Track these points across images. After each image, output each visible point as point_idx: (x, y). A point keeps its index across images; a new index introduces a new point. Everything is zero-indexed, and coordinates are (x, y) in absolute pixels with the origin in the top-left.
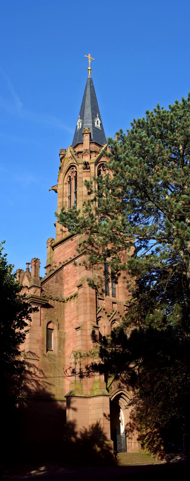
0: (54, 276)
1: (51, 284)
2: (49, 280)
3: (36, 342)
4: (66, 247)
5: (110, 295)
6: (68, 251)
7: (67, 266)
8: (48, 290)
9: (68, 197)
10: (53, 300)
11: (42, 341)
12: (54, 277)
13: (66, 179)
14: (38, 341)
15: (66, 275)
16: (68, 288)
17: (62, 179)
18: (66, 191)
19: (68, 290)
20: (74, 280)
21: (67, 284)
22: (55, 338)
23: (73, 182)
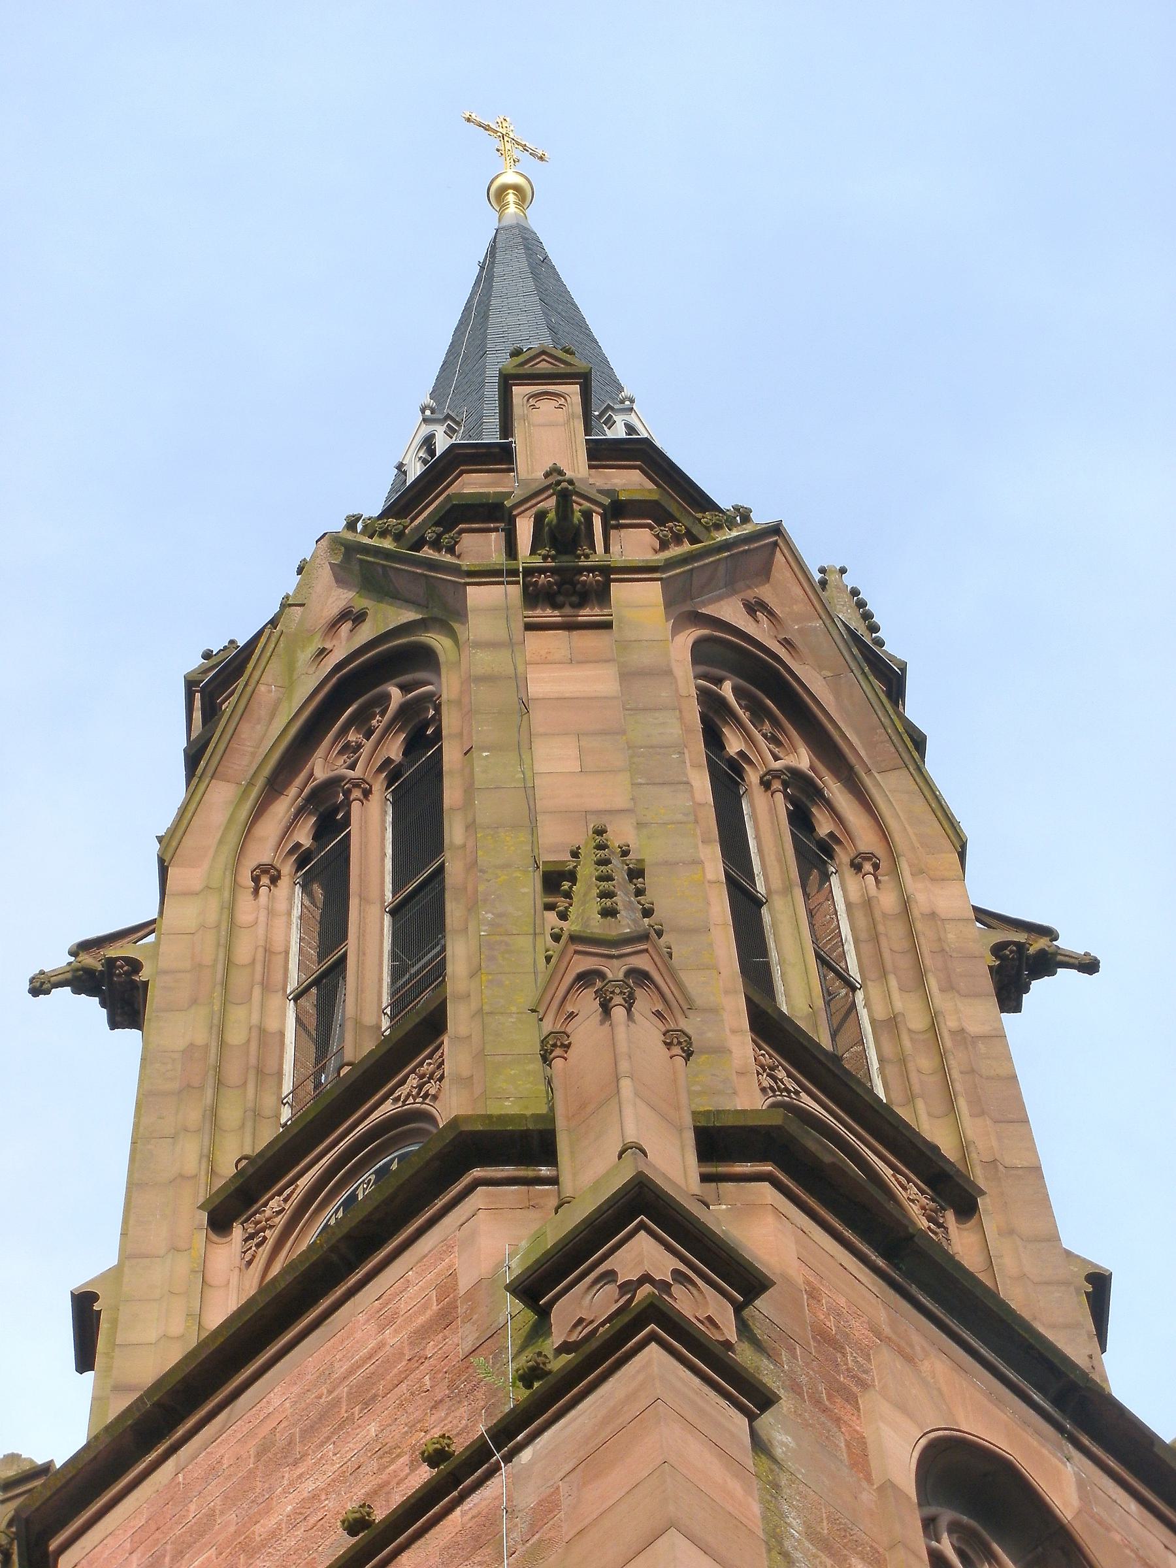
6: (309, 1486)
17: (221, 842)
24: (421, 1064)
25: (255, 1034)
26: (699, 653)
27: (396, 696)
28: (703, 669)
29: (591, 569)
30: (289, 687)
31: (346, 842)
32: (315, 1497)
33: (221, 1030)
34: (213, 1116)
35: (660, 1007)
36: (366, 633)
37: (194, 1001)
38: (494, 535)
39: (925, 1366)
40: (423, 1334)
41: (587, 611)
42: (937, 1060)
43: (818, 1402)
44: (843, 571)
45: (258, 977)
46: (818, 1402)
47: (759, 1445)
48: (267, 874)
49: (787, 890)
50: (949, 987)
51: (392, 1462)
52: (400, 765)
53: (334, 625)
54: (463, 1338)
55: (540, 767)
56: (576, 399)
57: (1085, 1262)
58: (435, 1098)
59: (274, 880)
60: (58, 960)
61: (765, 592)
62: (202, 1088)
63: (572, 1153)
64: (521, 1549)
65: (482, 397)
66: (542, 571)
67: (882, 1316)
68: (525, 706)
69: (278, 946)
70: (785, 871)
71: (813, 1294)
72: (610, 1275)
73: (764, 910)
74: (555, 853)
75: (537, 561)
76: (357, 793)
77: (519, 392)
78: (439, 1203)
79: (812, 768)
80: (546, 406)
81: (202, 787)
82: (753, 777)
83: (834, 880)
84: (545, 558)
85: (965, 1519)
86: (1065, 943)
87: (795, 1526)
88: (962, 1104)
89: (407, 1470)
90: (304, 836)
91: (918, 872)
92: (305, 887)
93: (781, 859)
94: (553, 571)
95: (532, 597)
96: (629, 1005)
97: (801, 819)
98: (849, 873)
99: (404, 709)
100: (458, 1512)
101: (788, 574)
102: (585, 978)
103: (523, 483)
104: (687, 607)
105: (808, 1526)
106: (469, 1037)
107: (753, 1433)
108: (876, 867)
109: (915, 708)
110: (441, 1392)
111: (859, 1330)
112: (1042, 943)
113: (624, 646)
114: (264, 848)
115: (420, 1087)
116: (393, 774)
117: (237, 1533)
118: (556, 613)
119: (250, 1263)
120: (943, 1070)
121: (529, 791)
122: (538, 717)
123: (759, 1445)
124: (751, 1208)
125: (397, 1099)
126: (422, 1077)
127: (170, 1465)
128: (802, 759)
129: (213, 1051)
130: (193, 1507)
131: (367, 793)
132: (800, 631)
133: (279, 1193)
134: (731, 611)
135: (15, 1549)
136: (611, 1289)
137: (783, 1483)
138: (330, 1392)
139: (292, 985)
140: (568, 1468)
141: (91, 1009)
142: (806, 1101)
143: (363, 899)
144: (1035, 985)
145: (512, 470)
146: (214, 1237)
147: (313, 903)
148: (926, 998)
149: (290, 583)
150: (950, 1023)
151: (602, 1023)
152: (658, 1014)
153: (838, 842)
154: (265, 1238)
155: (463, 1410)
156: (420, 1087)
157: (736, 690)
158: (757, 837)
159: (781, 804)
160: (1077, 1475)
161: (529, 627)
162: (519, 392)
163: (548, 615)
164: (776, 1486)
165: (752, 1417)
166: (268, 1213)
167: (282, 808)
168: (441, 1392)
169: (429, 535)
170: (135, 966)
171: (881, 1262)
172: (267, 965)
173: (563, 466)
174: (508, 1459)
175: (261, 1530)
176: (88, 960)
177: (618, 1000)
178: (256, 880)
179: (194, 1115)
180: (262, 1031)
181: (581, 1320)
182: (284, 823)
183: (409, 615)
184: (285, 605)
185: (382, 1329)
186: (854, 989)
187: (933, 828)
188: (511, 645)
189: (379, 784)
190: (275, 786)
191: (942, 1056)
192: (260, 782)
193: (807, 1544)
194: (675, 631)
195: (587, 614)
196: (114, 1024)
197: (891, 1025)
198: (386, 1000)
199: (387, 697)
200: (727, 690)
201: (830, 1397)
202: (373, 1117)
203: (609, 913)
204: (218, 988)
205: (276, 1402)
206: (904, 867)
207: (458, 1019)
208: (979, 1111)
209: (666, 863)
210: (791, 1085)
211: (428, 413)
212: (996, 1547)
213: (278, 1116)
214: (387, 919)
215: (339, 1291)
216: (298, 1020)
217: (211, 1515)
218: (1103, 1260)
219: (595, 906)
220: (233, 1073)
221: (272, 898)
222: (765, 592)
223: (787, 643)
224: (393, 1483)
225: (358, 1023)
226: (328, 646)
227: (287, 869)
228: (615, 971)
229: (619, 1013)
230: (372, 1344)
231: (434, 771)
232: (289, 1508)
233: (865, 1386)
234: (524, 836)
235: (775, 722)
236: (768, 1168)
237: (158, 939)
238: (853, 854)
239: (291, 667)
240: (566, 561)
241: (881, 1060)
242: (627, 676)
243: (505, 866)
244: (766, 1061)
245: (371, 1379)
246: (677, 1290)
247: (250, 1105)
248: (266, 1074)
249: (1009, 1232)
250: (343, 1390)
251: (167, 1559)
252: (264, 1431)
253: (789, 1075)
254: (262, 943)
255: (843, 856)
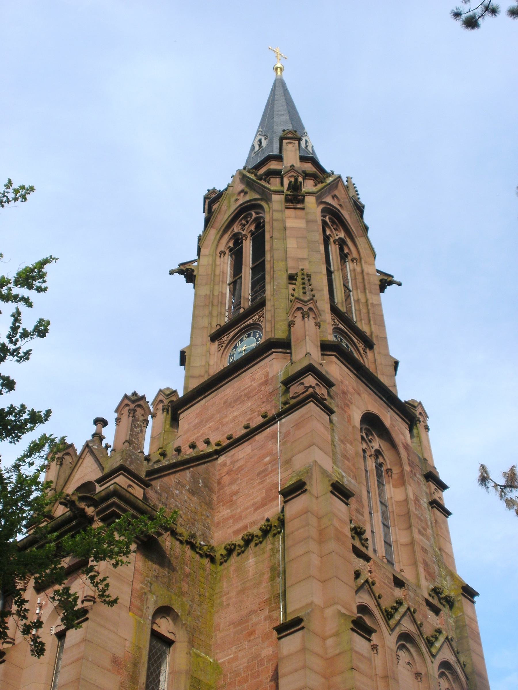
0: (187, 472)
1: (177, 492)
2: (172, 477)
3: (107, 663)
4: (228, 404)
5: (421, 560)
6: (236, 414)
7: (232, 452)
8: (166, 505)
9: (229, 285)
10: (181, 542)
11: (130, 666)
12: (188, 474)
13: (226, 242)
14: (115, 661)
15: (226, 479)
16: (232, 517)
17: (213, 243)
18: (223, 270)
19: (231, 521)
20: (262, 486)
21: (230, 502)
22: (173, 673)
23: (248, 247)
24: (259, 313)
25: (220, 294)
26: (323, 211)
27: (254, 215)
28: (323, 214)
29: (301, 195)
30: (229, 207)
31: (242, 248)
32: (236, 416)
33: (212, 291)
34: (211, 313)
35: (314, 316)
36: (247, 198)
37: (207, 284)
38: (278, 179)
39: (363, 395)
40: (261, 385)
41: (299, 205)
42: (367, 310)
43: (342, 408)
44: (352, 178)
45: (221, 279)
46: (342, 408)
47: (331, 421)
48: (223, 253)
49: (338, 270)
50: (370, 292)
51: (254, 413)
52: (254, 232)
53: (240, 193)
54: (269, 388)
55: (288, 246)
56: (297, 145)
57: (394, 359)
58: (262, 322)
59: (224, 255)
60: (176, 267)
61: (336, 192)
62: (209, 305)
63: (295, 351)
64: (282, 441)
65: (273, 131)
66: (290, 195)
67: (354, 384)
68: (285, 229)
69: (225, 272)
70: (338, 265)
71: (342, 382)
72: (303, 384)
73: (333, 275)
74: (291, 272)
75: (289, 193)
76: (244, 238)
77: (285, 142)
78: (265, 355)
79: (345, 237)
80: (290, 146)
81: (209, 230)
82: (332, 240)
83: (347, 263)
84: (291, 192)
85: (368, 427)
86: (395, 279)
87: (337, 439)
88: (372, 322)
89: (257, 416)
90: (231, 244)
91: (366, 262)
92: (231, 256)
93: (337, 262)
94: (292, 195)
95: (287, 200)
96: (308, 316)
97: (341, 249)
98: (350, 262)
99: (256, 219)
100: (268, 429)
101: (341, 187)
102: (299, 309)
103: (285, 167)
104: (320, 201)
105: (339, 438)
106: (271, 310)
107: (330, 419)
108: (356, 261)
109: (367, 219)
110: (265, 400)
111: (351, 390)
112: (390, 279)
113: (307, 214)
114: (222, 247)
115: (259, 318)
116: (252, 233)
117: (220, 420)
118: (292, 205)
119: (219, 351)
120: (368, 312)
121: (286, 251)
122: (288, 232)
123: (331, 421)
124: (331, 362)
125: (254, 320)
126: (259, 316)
127: (204, 400)
128: (342, 235)
129: (211, 297)
130: (209, 411)
131: (246, 238)
132: (344, 202)
133: (226, 335)
134: (329, 199)
135: (170, 408)
136: (302, 387)
137: (335, 429)
138: (240, 393)
139: (228, 282)
140: (292, 425)
141: (182, 278)
142: (341, 326)
143: (246, 266)
144: (388, 287)
145: (282, 161)
146: (212, 343)
147: (232, 259)
148: (366, 295)
149: (230, 180)
150: (370, 301)
151: (302, 320)
152: (314, 318)
153: (349, 254)
154: (223, 346)
155: (269, 405)
156: (259, 318)
157: (330, 218)
158: (332, 256)
159: (338, 246)
160: (390, 415)
161: (287, 208)
162: (285, 142)
163: (290, 205)
164: (333, 430)
165: (329, 416)
166: (224, 340)
167: (227, 237)
168: (265, 400)
169: (263, 177)
170: (193, 271)
171: (355, 372)
172: (223, 276)
173: (295, 165)
174: (279, 420)
175: (226, 420)
176: (182, 267)
177: (306, 316)
178: (221, 254)
179: (207, 312)
180: (222, 293)
181: (296, 392)
182: (227, 241)
183: (257, 196)
184: (229, 186)
185: (252, 381)
186: (350, 291)
187: (369, 251)
188: (282, 211)
189: (249, 236)
190: (225, 231)
191: (368, 310)
192: (222, 230)
193: (339, 442)
194: (318, 206)
195: (299, 206)
196: (187, 282)
197: (358, 301)
198: (250, 292)
199: (251, 215)
200: (327, 219)
201: (344, 406)
202: (248, 322)
203: (304, 293)
204: (212, 282)
205: (228, 392)
206: (363, 261)
207: (268, 304)
208: (375, 324)
209: (315, 272)
210: (338, 323)
211: (260, 132)
212: (373, 432)
213: (225, 314)
214: (251, 271)
215: (242, 370)
216: (230, 290)
217: (213, 414)
218: (397, 358)
219: (301, 291)
220: (215, 303)
221: (224, 259)
222: (336, 192)
223: (340, 205)
224: (254, 418)
225: (244, 297)
226: (238, 198)
227: (227, 252)
228: (306, 309)
229: (306, 319)
230: (249, 384)
231: (263, 235)
232: (231, 417)
233: (351, 403)
234: (284, 263)
235: (337, 225)
236: (334, 353)
237: (198, 264)
238: (352, 258)
239: (229, 202)
240: (295, 193)
241: (355, 310)
242: (308, 222)
243: (280, 270)
244: (333, 318)
245: (249, 392)
246: (317, 388)
247: (219, 311)
248: (223, 304)
249: (379, 353)
250: (243, 393)
251: (204, 422)
252: (226, 398)
253: (337, 320)
254: (221, 271)
255: (350, 258)
